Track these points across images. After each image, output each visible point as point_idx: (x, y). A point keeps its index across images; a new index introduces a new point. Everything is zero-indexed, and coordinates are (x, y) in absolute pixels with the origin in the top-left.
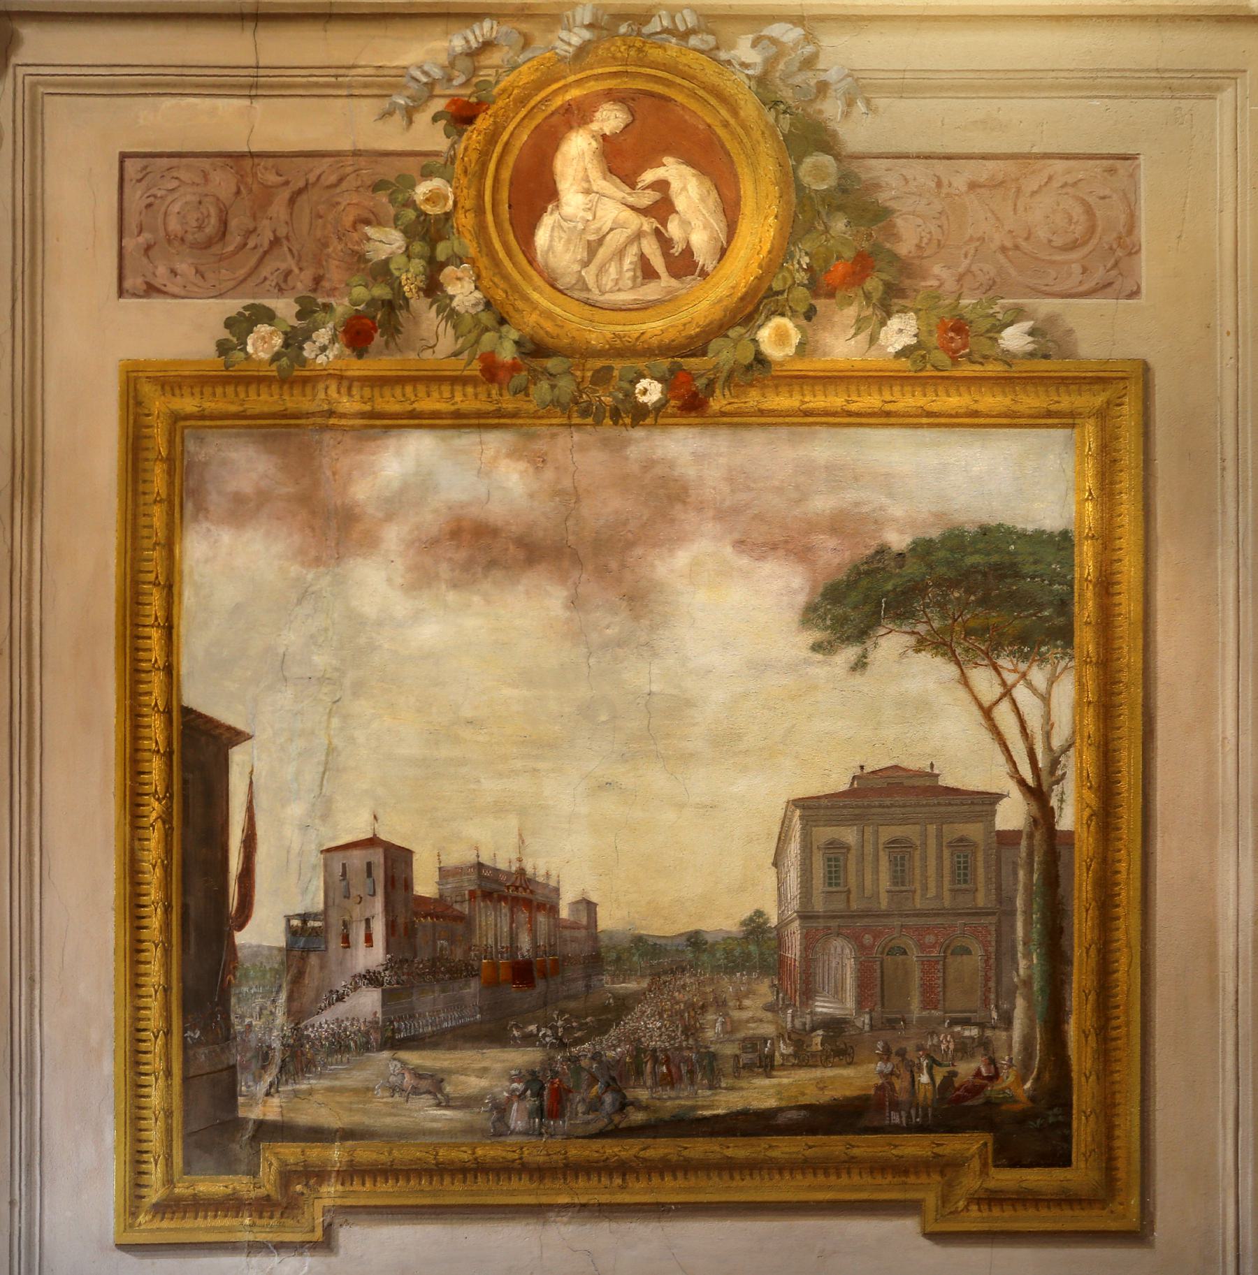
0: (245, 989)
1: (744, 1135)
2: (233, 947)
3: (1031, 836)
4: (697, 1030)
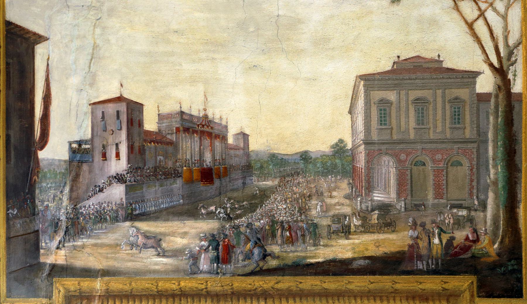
0: (44, 185)
1: (335, 274)
3: (497, 96)
4: (306, 210)
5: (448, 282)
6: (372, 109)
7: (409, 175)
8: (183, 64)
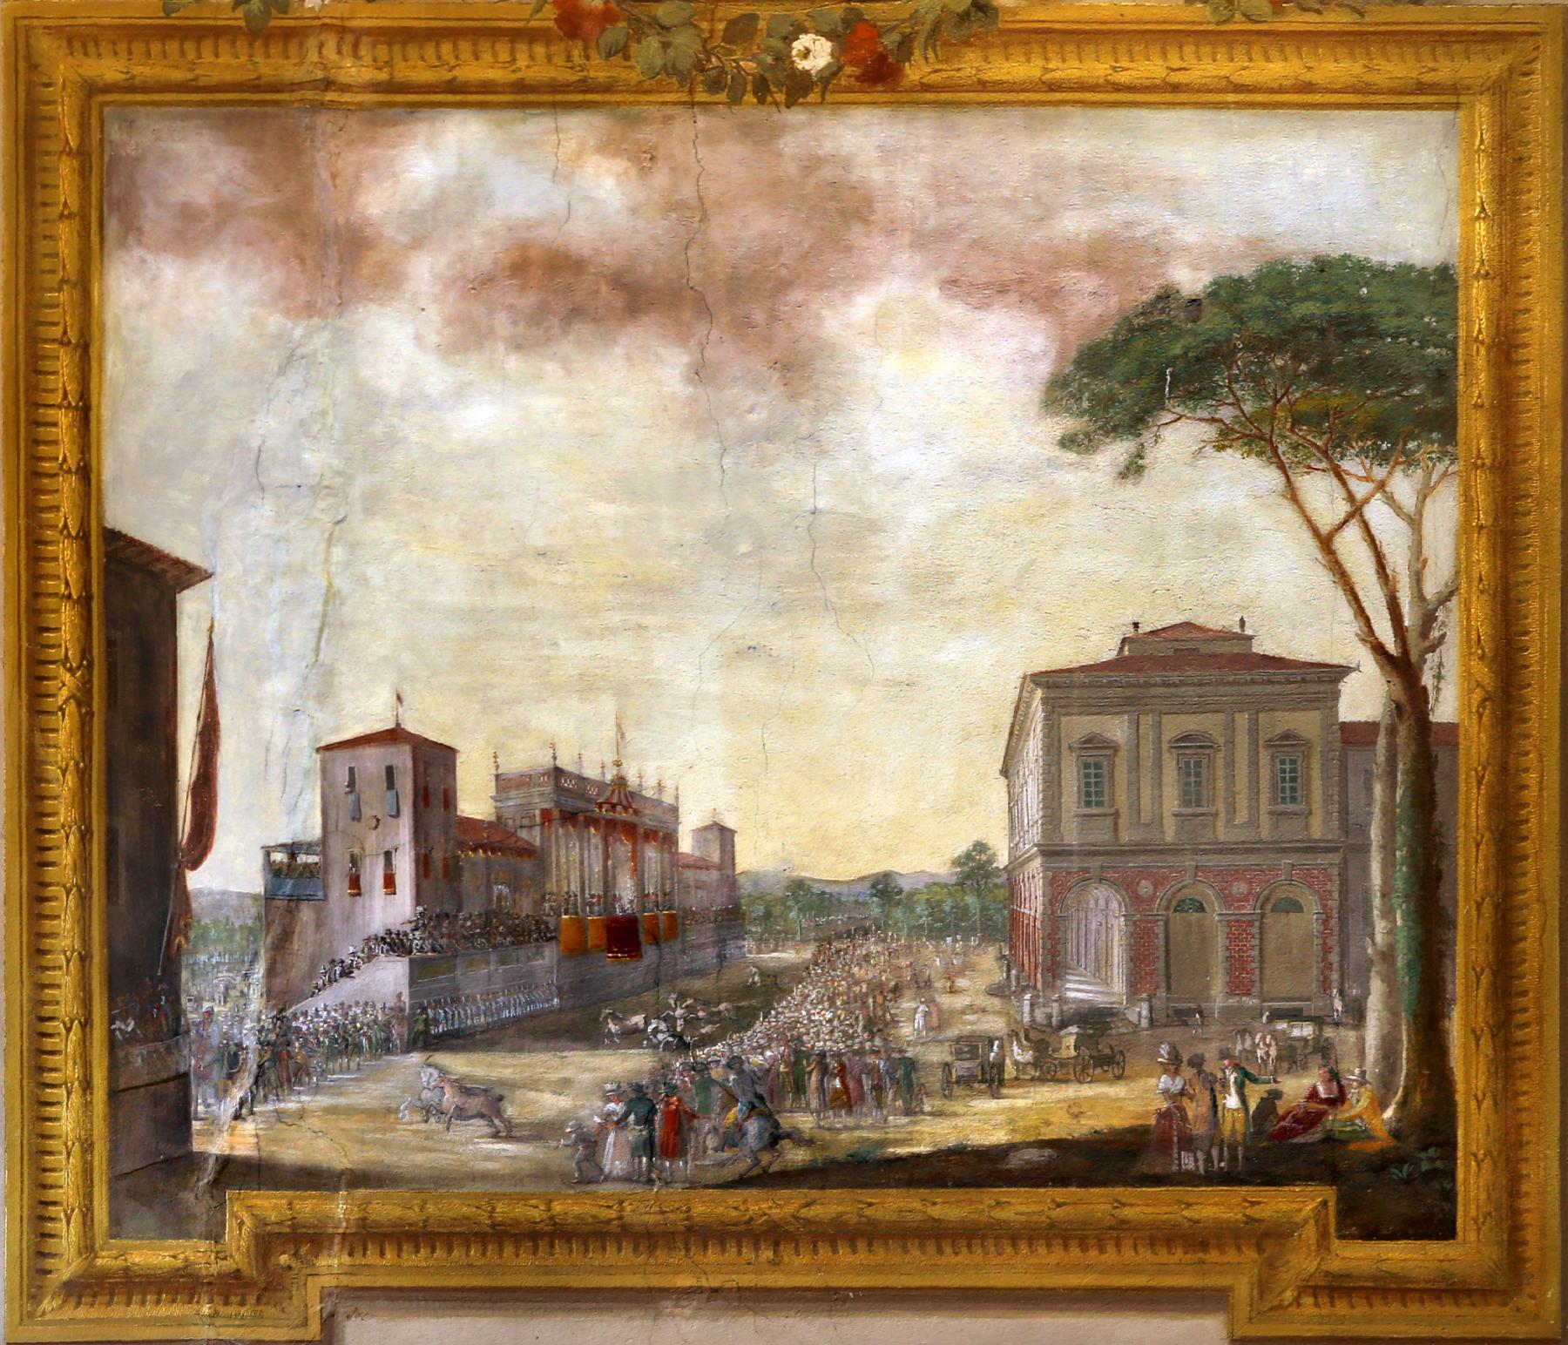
0: (203, 958)
1: (960, 1184)
2: (184, 896)
3: (1392, 732)
4: (886, 1024)
5: (1258, 1203)
6: (1063, 764)
7: (1162, 936)
8: (562, 642)
